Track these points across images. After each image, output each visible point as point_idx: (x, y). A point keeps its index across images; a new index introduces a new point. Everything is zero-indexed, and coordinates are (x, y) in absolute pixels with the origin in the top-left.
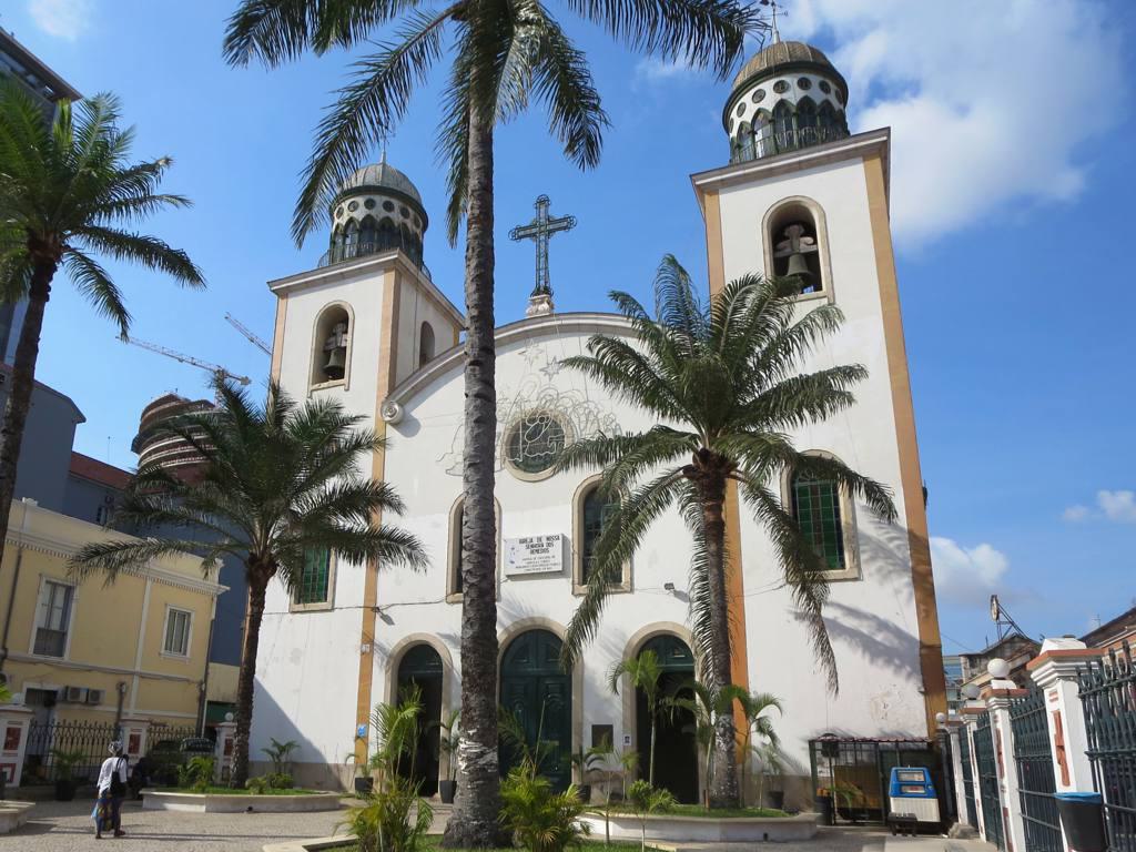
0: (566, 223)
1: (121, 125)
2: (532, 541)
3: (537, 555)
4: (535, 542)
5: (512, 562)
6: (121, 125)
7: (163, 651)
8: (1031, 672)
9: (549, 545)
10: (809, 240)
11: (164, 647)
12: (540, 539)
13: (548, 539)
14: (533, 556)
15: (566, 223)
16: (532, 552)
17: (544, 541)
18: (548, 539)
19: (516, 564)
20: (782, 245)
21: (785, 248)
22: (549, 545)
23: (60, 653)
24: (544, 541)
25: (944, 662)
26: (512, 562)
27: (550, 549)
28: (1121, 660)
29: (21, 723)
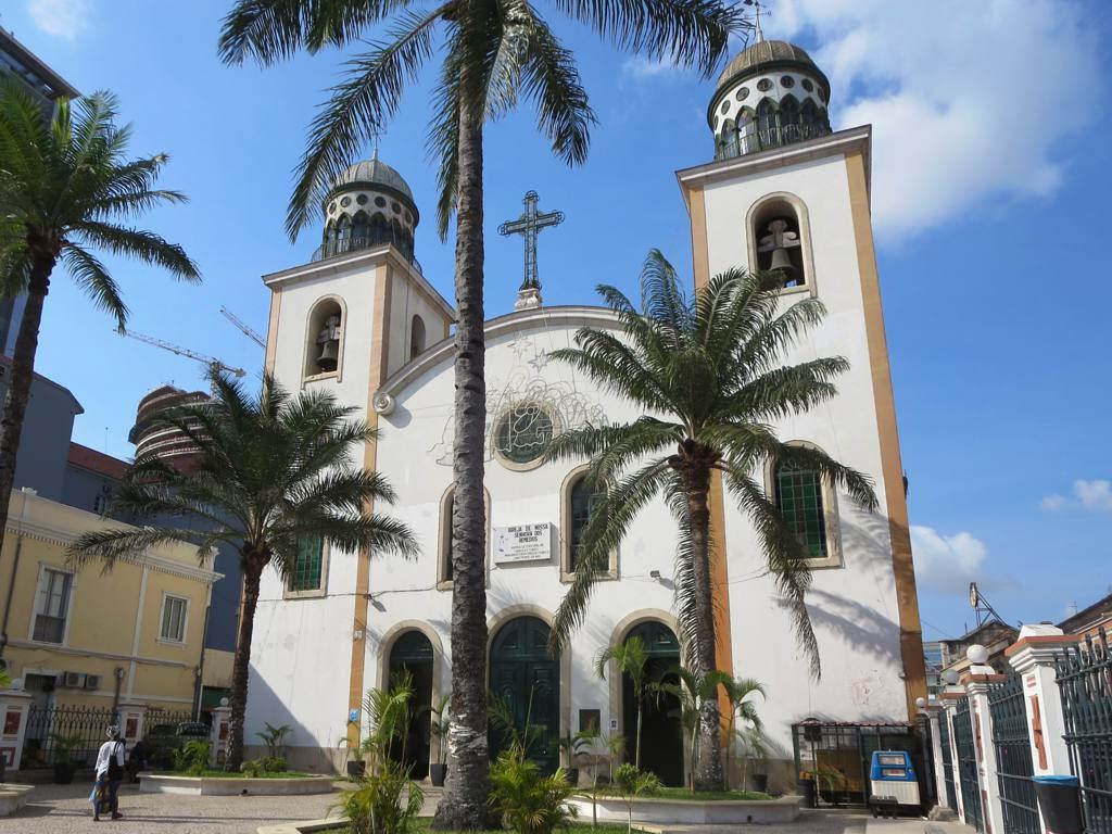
1: (118, 123)
2: (520, 529)
3: (525, 543)
4: (524, 530)
5: (501, 550)
6: (118, 123)
9: (537, 533)
12: (528, 528)
13: (536, 527)
16: (521, 541)
17: (533, 530)
18: (536, 527)
22: (537, 533)
24: (533, 530)
26: (501, 550)
27: (538, 537)
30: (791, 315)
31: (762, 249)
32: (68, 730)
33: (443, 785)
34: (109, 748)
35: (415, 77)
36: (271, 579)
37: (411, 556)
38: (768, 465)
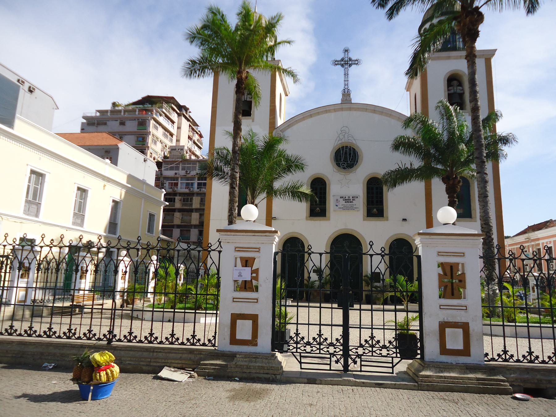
0: (336, 63)
1: (501, 128)
2: (345, 197)
3: (347, 204)
4: (347, 198)
5: (337, 206)
6: (501, 128)
7: (147, 233)
8: (415, 240)
9: (353, 200)
10: (460, 88)
11: (147, 231)
12: (349, 197)
13: (353, 197)
14: (346, 204)
15: (336, 63)
16: (346, 202)
17: (351, 198)
18: (353, 197)
19: (339, 207)
20: (450, 88)
21: (451, 90)
22: (353, 200)
23: (37, 215)
24: (351, 198)
25: (417, 244)
26: (337, 206)
27: (354, 201)
28: (353, 206)
29: (234, 300)
30: (78, 249)
31: (450, 92)
32: (54, 275)
33: (91, 400)
34: (180, 280)
35: (398, 186)
36: (442, 273)
37: (291, 45)
38: (115, 375)
